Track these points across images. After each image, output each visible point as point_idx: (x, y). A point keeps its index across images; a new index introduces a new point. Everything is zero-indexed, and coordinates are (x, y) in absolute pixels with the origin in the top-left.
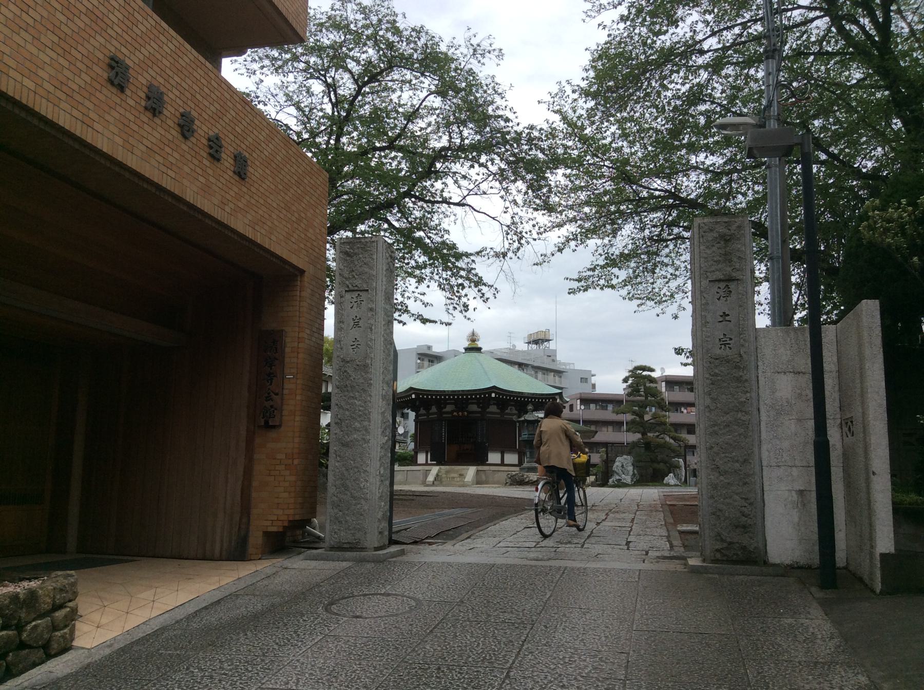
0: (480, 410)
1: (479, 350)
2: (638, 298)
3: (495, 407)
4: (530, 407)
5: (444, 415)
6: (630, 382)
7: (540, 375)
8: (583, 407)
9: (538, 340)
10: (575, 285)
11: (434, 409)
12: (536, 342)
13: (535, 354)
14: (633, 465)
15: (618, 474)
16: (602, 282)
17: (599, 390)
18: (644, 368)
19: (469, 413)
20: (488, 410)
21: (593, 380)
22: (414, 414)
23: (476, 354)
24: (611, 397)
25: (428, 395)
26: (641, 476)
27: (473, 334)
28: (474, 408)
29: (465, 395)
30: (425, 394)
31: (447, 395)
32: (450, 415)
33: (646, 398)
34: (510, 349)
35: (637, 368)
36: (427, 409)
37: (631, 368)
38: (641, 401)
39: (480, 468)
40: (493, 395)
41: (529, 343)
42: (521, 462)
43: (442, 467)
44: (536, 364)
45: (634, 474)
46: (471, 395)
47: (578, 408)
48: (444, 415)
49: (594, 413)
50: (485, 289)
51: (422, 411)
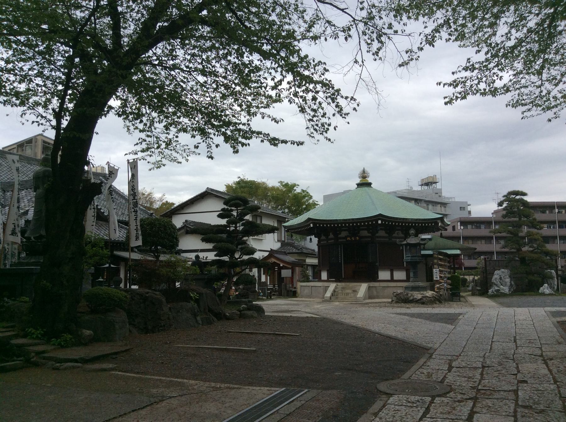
0: (370, 235)
1: (369, 185)
2: (523, 105)
3: (384, 232)
4: (412, 231)
5: (340, 240)
6: (505, 205)
7: (430, 207)
8: (462, 228)
9: (429, 183)
10: (450, 91)
11: (331, 236)
12: (427, 184)
13: (427, 193)
14: (510, 277)
15: (497, 285)
16: (482, 86)
17: (474, 215)
18: (517, 193)
19: (361, 237)
20: (377, 235)
21: (469, 208)
22: (317, 239)
23: (366, 189)
24: (478, 219)
25: (331, 224)
26: (517, 285)
27: (364, 171)
28: (365, 233)
29: (355, 222)
30: (329, 224)
31: (339, 223)
32: (345, 240)
33: (520, 219)
34: (408, 190)
35: (510, 193)
36: (327, 235)
37: (505, 193)
38: (515, 221)
39: (373, 284)
40: (380, 222)
41: (422, 185)
42: (408, 280)
43: (339, 284)
44: (427, 199)
45: (511, 285)
46: (360, 222)
47: (459, 228)
48: (340, 240)
49: (471, 231)
50: (342, 102)
51: (323, 237)
